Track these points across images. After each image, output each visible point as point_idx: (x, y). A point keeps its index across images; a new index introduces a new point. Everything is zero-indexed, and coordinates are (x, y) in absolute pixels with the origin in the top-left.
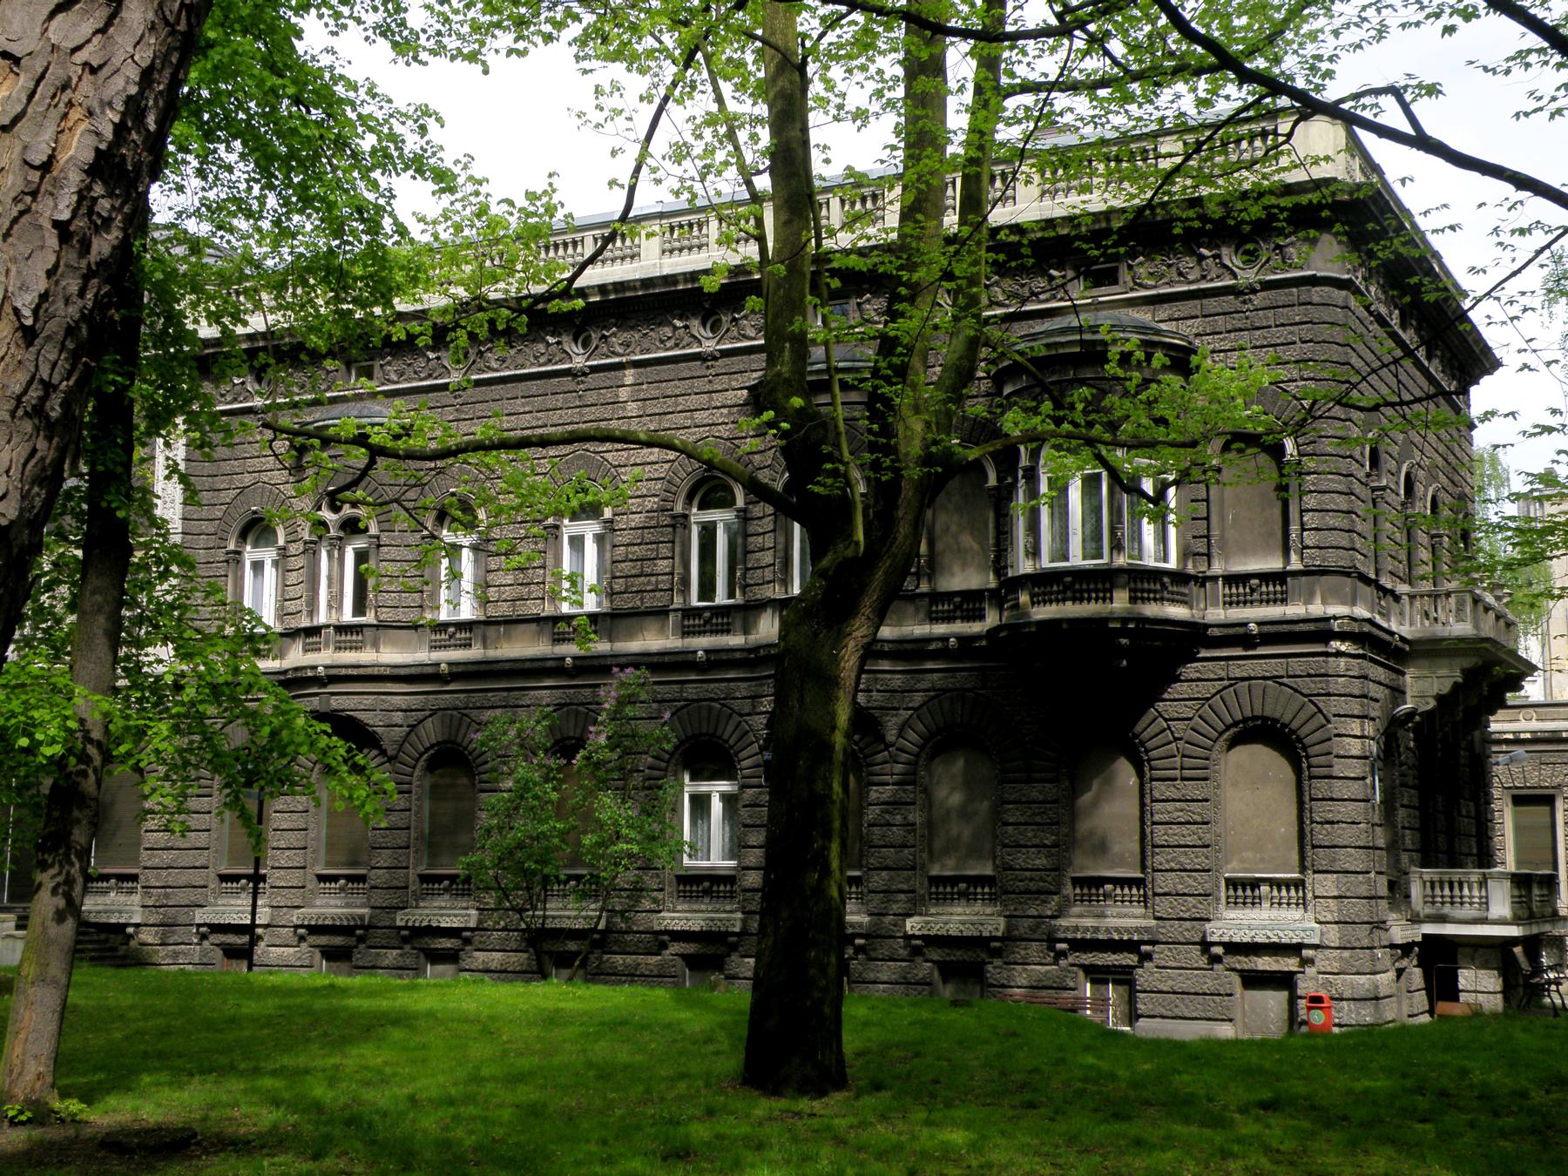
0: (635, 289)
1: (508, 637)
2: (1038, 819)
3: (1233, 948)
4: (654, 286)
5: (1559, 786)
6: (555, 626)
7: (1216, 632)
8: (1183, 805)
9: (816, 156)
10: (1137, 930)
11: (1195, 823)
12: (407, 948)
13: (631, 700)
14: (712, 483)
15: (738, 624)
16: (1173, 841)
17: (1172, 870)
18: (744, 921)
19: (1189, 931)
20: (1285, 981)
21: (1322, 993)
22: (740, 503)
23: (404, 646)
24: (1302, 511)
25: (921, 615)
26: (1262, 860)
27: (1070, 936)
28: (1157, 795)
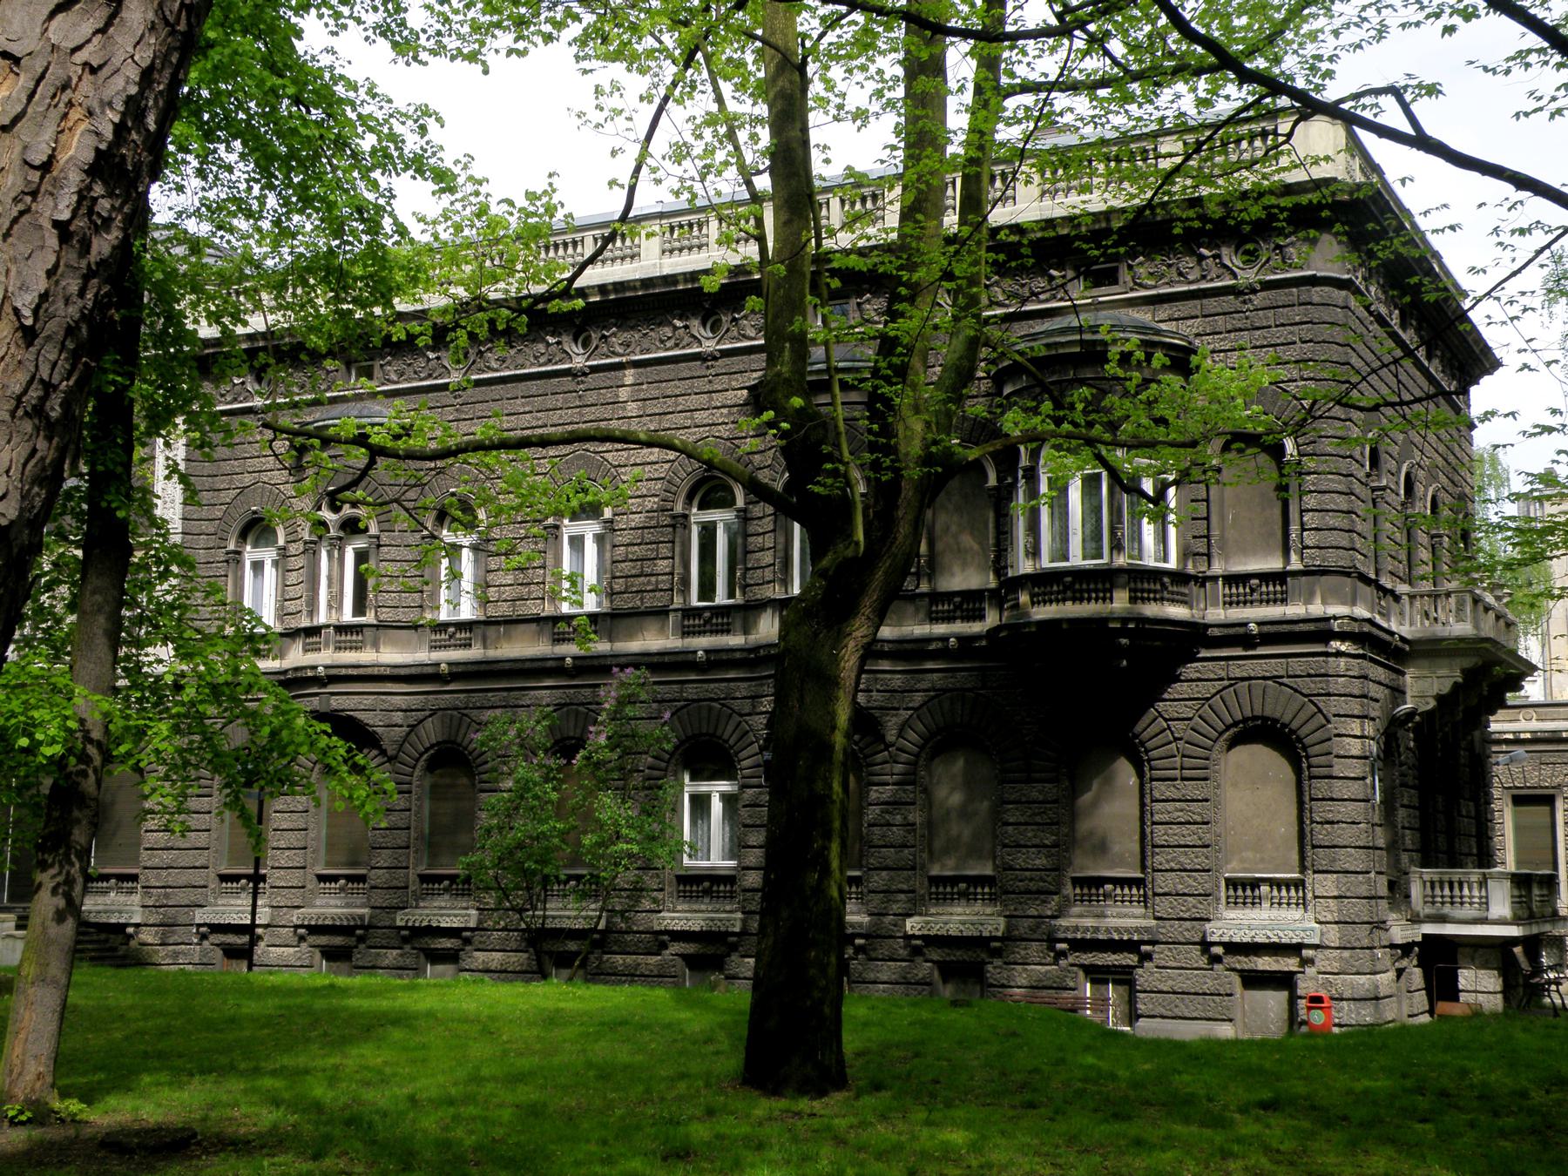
0: (635, 289)
1: (508, 637)
2: (1038, 819)
3: (1233, 948)
4: (654, 286)
5: (1559, 786)
6: (555, 626)
7: (1216, 632)
8: (1183, 805)
9: (816, 156)
10: (1137, 930)
11: (1195, 823)
12: (407, 948)
13: (631, 700)
14: (712, 483)
15: (738, 624)
16: (1173, 841)
17: (1172, 870)
18: (744, 921)
19: (1189, 931)
20: (1285, 981)
21: (1322, 993)
22: (740, 503)
23: (404, 646)
24: (1302, 511)
25: (921, 615)
26: (1262, 860)
27: (1070, 936)
28: (1157, 795)
